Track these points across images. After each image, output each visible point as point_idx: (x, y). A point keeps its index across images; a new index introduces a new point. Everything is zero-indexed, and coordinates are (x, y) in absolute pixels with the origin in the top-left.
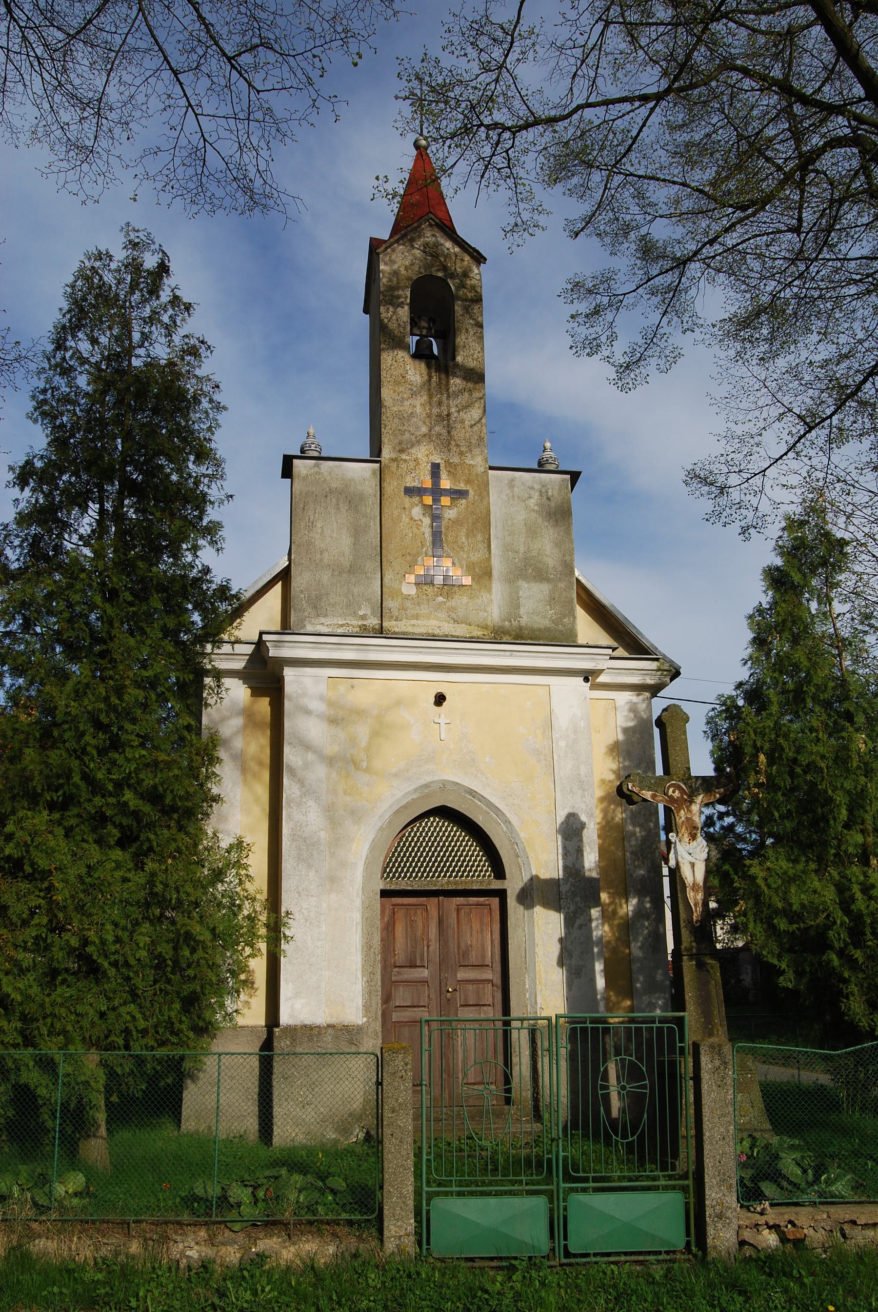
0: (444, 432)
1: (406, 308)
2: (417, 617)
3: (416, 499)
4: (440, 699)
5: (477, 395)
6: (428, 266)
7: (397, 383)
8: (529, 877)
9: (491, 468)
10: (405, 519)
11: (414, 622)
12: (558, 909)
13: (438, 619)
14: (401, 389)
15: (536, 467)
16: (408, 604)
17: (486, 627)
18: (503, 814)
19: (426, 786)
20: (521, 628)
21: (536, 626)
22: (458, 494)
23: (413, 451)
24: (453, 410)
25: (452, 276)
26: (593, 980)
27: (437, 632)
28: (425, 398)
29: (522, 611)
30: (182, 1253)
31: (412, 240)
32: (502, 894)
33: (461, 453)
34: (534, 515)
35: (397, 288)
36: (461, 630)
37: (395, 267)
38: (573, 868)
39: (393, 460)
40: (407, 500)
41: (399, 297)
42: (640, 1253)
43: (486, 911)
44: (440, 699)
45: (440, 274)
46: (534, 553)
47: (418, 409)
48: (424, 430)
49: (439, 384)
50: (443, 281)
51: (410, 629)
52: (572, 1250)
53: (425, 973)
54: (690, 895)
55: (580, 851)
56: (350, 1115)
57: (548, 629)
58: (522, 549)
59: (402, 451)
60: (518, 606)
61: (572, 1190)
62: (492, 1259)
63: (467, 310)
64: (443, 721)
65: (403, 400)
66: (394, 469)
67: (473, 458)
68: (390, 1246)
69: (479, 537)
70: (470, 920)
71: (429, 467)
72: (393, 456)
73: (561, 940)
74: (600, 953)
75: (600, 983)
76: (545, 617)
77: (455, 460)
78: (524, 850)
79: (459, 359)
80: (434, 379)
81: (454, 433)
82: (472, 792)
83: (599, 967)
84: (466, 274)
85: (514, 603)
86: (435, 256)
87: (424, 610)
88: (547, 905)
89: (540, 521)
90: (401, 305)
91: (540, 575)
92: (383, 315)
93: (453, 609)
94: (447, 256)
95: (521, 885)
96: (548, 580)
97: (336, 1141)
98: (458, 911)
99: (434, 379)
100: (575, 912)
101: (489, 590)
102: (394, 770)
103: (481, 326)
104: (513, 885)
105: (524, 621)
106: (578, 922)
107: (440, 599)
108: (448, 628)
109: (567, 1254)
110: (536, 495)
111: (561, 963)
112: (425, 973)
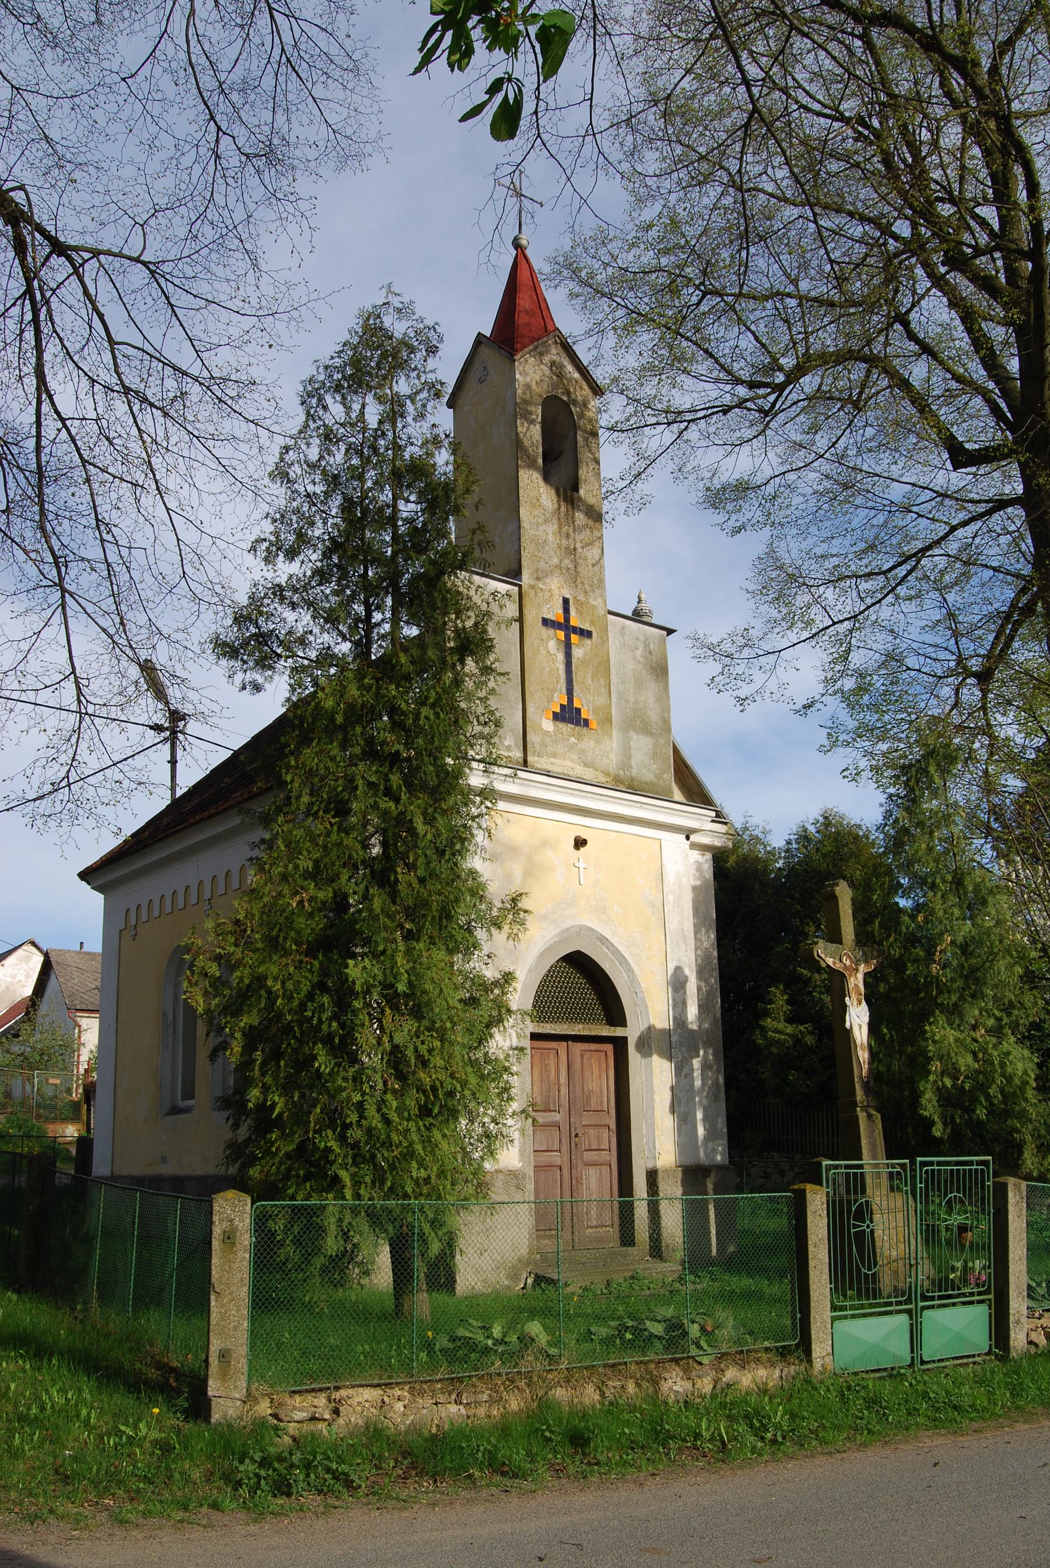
0: (571, 566)
1: (538, 426)
2: (554, 755)
3: (551, 632)
4: (580, 843)
5: (596, 534)
6: (555, 386)
7: (533, 506)
8: (646, 1026)
9: (610, 613)
10: (543, 652)
11: (552, 760)
12: (670, 1059)
13: (571, 760)
14: (537, 512)
15: (630, 614)
16: (548, 741)
17: (608, 774)
18: (628, 963)
19: (568, 930)
20: (632, 779)
21: (644, 779)
22: (586, 634)
23: (547, 580)
24: (578, 545)
25: (575, 402)
26: (695, 1126)
27: (571, 773)
28: (556, 526)
29: (633, 762)
30: (670, 1389)
31: (541, 354)
32: (621, 1045)
33: (586, 592)
34: (640, 667)
35: (530, 403)
36: (589, 774)
37: (528, 380)
38: (680, 1021)
39: (532, 587)
40: (544, 629)
41: (531, 413)
42: (962, 1357)
43: (603, 1057)
44: (580, 843)
45: (565, 398)
46: (641, 705)
47: (551, 538)
48: (556, 561)
49: (567, 515)
50: (566, 405)
51: (550, 768)
52: (925, 1359)
53: (557, 1117)
54: (860, 1053)
55: (684, 1003)
56: (520, 1261)
57: (652, 783)
58: (632, 700)
59: (538, 579)
60: (629, 757)
61: (923, 1308)
62: (873, 1371)
63: (586, 440)
64: (581, 865)
65: (538, 525)
66: (532, 596)
67: (595, 599)
68: (817, 1364)
69: (602, 682)
70: (591, 1066)
71: (561, 601)
72: (532, 582)
73: (672, 1088)
74: (700, 1101)
75: (701, 1131)
76: (650, 771)
77: (581, 597)
78: (643, 999)
79: (582, 492)
80: (563, 509)
81: (579, 569)
82: (603, 940)
83: (699, 1115)
84: (585, 405)
85: (626, 753)
86: (560, 376)
87: (560, 749)
88: (661, 1054)
89: (644, 673)
90: (532, 422)
91: (645, 729)
92: (520, 429)
93: (582, 752)
94: (570, 380)
95: (638, 1034)
96: (652, 734)
97: (508, 1287)
98: (582, 1056)
99: (563, 509)
100: (682, 1061)
101: (611, 737)
102: (543, 912)
103: (598, 462)
104: (632, 1032)
105: (635, 772)
106: (685, 1071)
107: (573, 739)
108: (579, 771)
109: (923, 1362)
110: (641, 647)
111: (673, 1110)
112: (557, 1117)
